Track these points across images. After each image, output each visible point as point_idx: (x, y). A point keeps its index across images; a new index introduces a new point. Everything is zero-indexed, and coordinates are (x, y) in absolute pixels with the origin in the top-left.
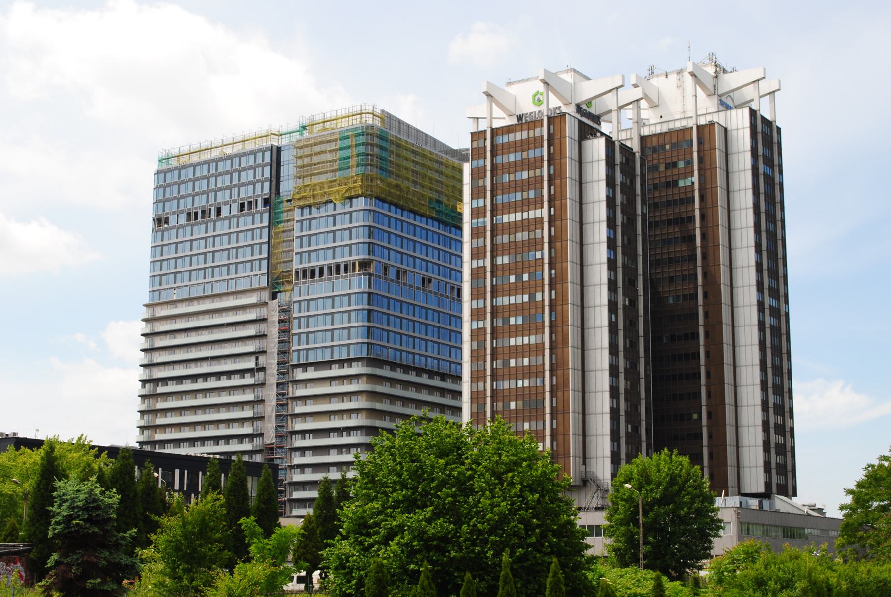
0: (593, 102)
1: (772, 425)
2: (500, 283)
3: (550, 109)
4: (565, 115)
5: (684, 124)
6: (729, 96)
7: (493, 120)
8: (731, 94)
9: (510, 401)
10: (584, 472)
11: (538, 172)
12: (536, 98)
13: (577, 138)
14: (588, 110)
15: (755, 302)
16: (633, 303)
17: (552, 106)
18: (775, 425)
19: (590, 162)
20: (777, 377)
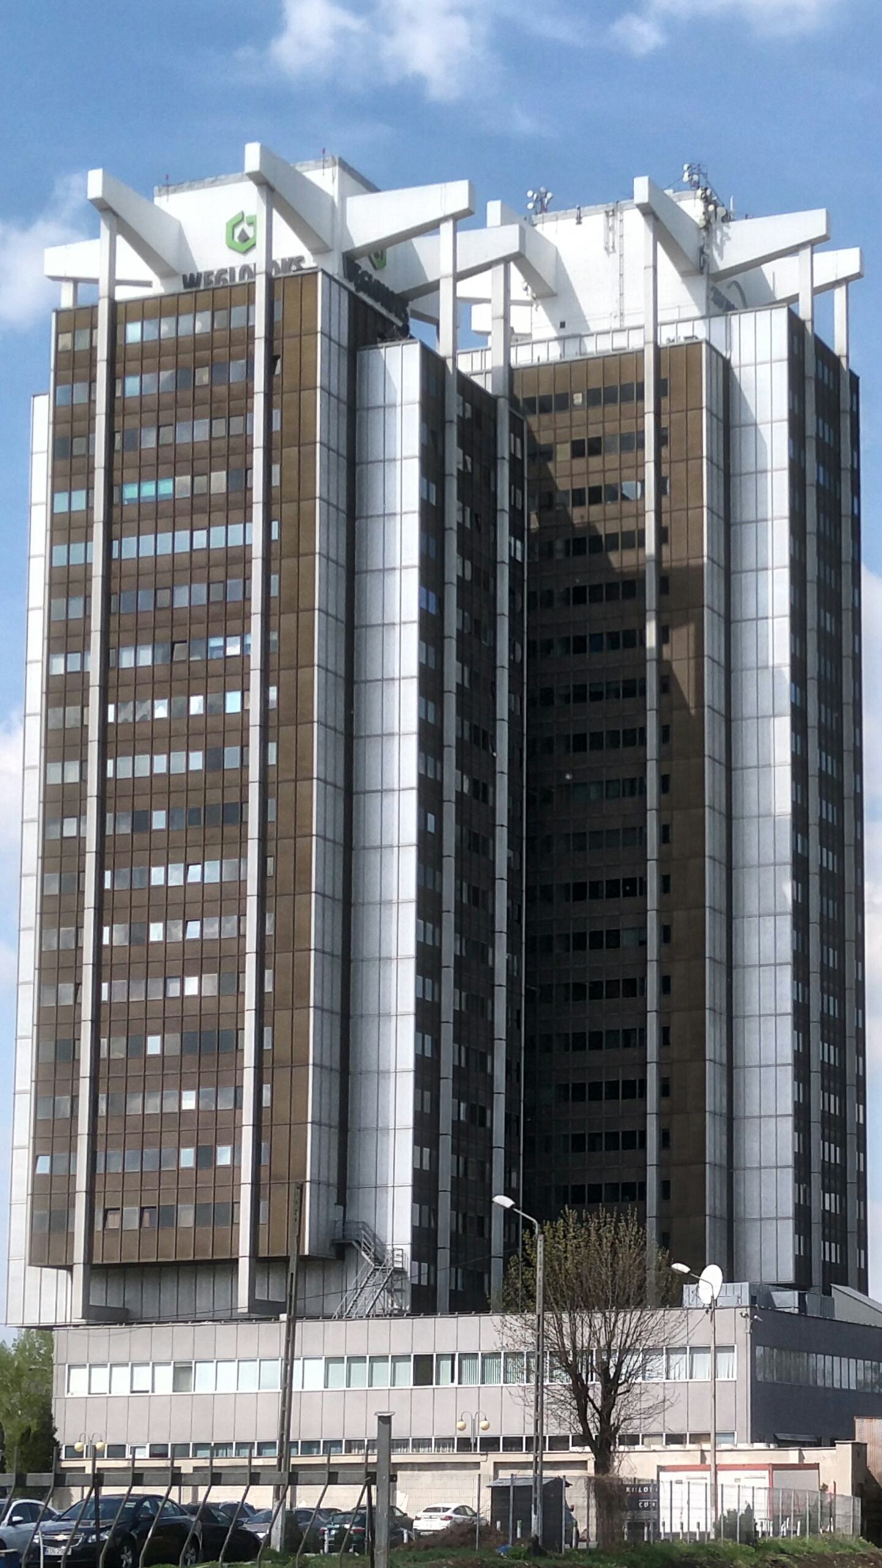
0: (389, 252)
1: (815, 1116)
2: (123, 885)
3: (275, 263)
4: (316, 273)
5: (620, 342)
6: (736, 283)
7: (80, 1488)
8: (738, 278)
9: (147, 1034)
10: (340, 1224)
11: (236, 423)
12: (238, 231)
13: (345, 342)
14: (376, 276)
15: (789, 1209)
16: (482, 790)
17: (278, 256)
18: (823, 1117)
19: (375, 848)
20: (832, 1097)
